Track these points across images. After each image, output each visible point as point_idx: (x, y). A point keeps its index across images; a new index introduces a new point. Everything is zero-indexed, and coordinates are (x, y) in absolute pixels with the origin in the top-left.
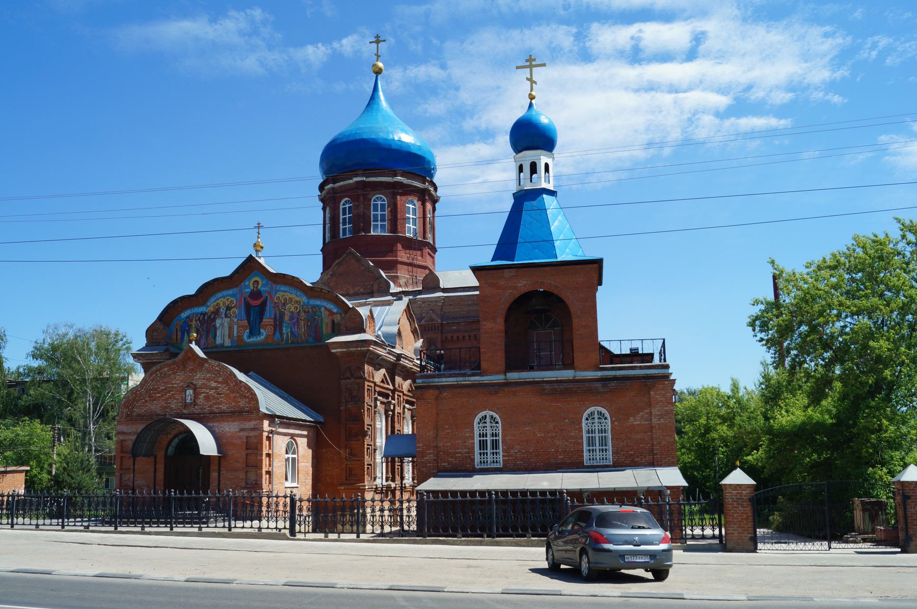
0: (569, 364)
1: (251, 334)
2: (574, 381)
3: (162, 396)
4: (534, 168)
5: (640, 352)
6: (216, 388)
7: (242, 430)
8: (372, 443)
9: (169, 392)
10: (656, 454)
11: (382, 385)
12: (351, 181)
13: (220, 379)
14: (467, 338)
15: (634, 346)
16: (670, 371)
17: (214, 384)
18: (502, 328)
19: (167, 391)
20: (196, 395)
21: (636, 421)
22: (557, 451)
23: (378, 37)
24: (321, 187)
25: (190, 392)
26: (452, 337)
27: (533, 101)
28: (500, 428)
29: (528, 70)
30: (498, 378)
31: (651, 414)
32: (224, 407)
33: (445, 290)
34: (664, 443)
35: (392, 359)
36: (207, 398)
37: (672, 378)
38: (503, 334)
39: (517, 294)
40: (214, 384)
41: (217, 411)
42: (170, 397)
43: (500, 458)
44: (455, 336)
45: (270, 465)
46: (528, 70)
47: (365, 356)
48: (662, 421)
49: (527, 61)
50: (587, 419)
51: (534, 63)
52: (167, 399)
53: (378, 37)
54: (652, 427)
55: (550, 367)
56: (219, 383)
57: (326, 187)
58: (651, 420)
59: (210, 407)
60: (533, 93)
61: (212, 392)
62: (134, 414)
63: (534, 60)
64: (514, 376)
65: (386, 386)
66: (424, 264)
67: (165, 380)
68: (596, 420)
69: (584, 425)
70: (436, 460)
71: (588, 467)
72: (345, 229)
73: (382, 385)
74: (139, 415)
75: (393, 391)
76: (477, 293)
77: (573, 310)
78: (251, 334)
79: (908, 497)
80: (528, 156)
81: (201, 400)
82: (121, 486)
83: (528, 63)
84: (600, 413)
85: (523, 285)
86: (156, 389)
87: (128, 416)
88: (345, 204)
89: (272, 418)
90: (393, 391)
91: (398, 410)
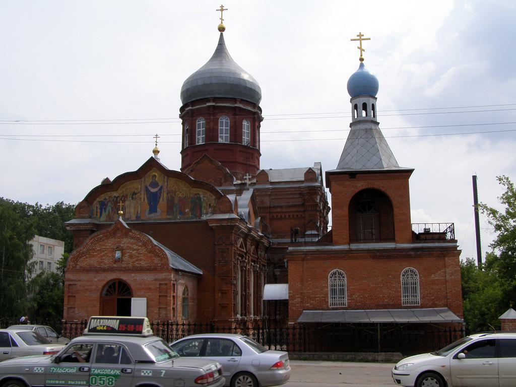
0: (392, 239)
1: (151, 212)
2: (395, 250)
3: (98, 254)
4: (365, 107)
5: (431, 232)
6: (138, 250)
7: (156, 280)
8: (235, 290)
10: (449, 299)
11: (240, 249)
12: (203, 106)
13: (140, 244)
14: (287, 217)
15: (427, 227)
17: (135, 247)
18: (347, 214)
20: (123, 254)
22: (383, 297)
23: (222, 6)
24: (182, 109)
26: (281, 216)
27: (363, 62)
28: (346, 281)
29: (359, 41)
30: (345, 247)
33: (272, 183)
34: (454, 291)
35: (246, 231)
36: (131, 256)
37: (458, 249)
39: (357, 191)
40: (135, 247)
41: (138, 265)
42: (104, 255)
43: (346, 300)
44: (279, 215)
45: (174, 304)
46: (359, 41)
47: (233, 229)
49: (358, 36)
50: (331, 277)
51: (362, 37)
52: (102, 256)
53: (222, 6)
54: (446, 281)
55: (370, 240)
56: (139, 246)
57: (187, 109)
60: (363, 57)
63: (363, 35)
64: (354, 246)
65: (242, 250)
66: (253, 164)
67: (100, 243)
68: (337, 278)
69: (401, 279)
70: (302, 302)
72: (200, 140)
73: (240, 249)
75: (246, 254)
77: (394, 203)
78: (151, 212)
80: (360, 101)
81: (126, 258)
83: (359, 38)
84: (340, 274)
85: (361, 185)
86: (94, 250)
87: (74, 267)
88: (201, 122)
89: (177, 271)
90: (246, 254)
91: (248, 267)
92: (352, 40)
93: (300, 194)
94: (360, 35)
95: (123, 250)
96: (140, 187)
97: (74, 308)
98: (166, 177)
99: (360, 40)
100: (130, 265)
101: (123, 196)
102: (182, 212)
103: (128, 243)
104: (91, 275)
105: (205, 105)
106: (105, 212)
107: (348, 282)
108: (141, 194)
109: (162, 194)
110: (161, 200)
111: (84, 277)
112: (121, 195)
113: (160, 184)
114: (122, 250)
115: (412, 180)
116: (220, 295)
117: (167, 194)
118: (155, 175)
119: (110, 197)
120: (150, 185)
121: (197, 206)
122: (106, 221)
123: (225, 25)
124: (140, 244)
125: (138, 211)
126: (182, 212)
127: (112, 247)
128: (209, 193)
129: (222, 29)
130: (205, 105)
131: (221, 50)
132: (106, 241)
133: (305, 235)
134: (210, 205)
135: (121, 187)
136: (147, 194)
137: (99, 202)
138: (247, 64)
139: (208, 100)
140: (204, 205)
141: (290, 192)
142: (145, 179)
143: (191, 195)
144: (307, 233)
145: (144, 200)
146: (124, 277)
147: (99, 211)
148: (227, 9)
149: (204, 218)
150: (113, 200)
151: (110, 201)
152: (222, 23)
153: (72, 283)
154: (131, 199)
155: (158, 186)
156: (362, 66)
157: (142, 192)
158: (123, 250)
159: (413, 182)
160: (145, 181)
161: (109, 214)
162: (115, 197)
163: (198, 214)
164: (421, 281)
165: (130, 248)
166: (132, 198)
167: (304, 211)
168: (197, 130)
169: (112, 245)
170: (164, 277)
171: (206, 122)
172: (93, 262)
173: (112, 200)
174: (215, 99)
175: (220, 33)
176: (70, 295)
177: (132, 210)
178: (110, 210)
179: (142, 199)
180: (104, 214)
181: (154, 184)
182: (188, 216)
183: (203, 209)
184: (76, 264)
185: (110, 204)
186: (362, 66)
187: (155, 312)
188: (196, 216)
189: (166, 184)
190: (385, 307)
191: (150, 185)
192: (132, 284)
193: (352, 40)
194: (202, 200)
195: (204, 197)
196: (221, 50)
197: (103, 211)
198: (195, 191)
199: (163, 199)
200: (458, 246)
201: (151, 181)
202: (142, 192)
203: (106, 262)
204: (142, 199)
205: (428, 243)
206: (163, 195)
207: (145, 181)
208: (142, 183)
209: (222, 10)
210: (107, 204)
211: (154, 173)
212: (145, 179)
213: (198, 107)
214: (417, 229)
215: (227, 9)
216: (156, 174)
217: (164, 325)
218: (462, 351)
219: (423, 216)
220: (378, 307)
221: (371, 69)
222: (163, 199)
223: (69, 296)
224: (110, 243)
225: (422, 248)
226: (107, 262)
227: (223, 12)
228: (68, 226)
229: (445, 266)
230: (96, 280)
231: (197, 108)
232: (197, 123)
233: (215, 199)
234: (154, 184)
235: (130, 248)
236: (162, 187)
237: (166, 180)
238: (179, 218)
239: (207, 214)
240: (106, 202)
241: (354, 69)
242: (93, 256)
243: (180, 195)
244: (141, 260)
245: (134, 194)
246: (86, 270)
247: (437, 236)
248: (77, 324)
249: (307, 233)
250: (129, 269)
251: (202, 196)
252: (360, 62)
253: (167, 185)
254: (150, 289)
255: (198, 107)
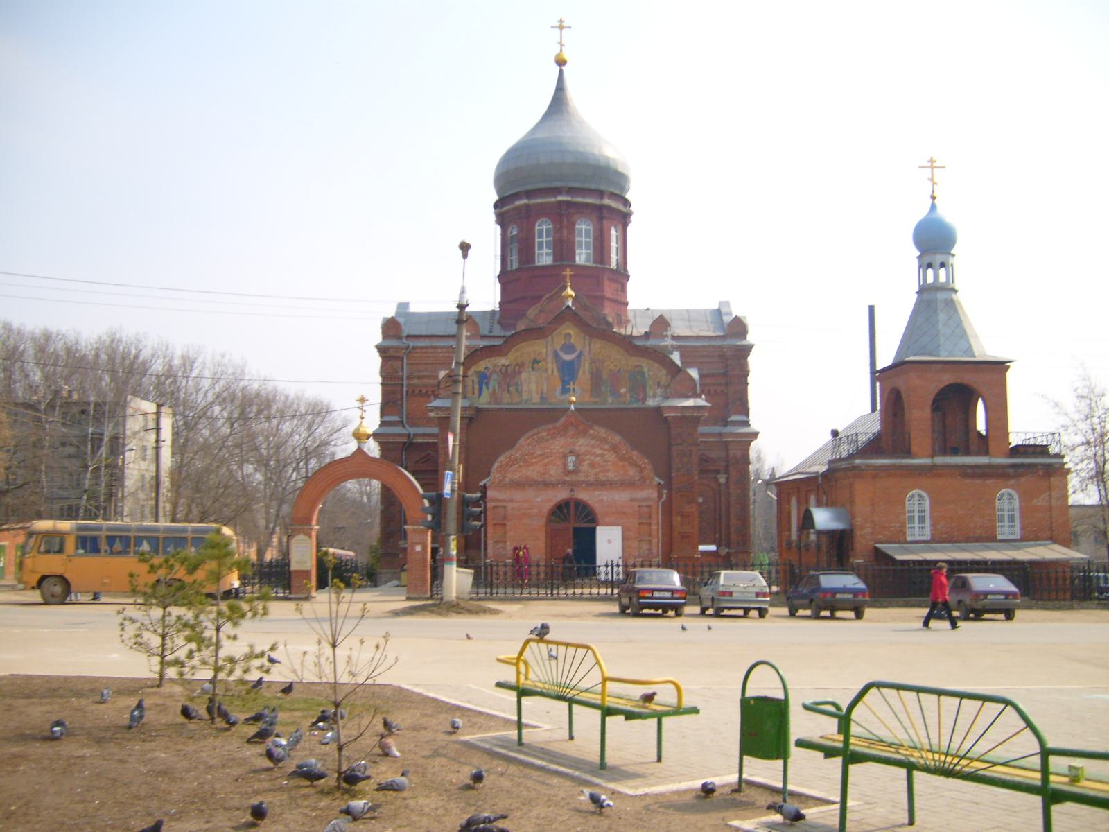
2: (990, 466)
6: (602, 456)
9: (547, 457)
16: (1065, 460)
17: (599, 452)
19: (544, 456)
21: (1040, 502)
23: (561, 21)
25: (571, 459)
30: (926, 461)
31: (1050, 496)
32: (611, 475)
36: (592, 465)
38: (930, 422)
40: (599, 452)
41: (603, 479)
48: (1059, 503)
52: (545, 465)
53: (561, 21)
56: (605, 450)
58: (1050, 501)
59: (596, 474)
61: (598, 459)
62: (507, 480)
64: (940, 460)
70: (872, 533)
71: (1002, 541)
74: (512, 481)
76: (878, 384)
79: (384, 637)
81: (585, 467)
82: (254, 579)
85: (947, 379)
86: (532, 454)
92: (920, 167)
93: (720, 356)
94: (932, 161)
95: (579, 455)
96: (544, 351)
97: (505, 542)
98: (587, 338)
99: (932, 167)
100: (592, 479)
101: (517, 365)
102: (615, 393)
103: (588, 445)
104: (529, 493)
105: (553, 200)
106: (488, 388)
107: (931, 507)
108: (547, 363)
109: (582, 364)
110: (580, 373)
111: (518, 495)
112: (514, 363)
113: (579, 348)
114: (578, 456)
115: (1010, 375)
116: (679, 519)
117: (591, 364)
118: (569, 335)
119: (495, 366)
120: (561, 349)
121: (639, 386)
122: (489, 403)
123: (566, 56)
124: (606, 447)
125: (542, 390)
126: (615, 393)
127: (561, 451)
128: (656, 365)
129: (561, 62)
130: (553, 200)
131: (559, 102)
132: (551, 442)
133: (727, 422)
134: (659, 383)
135: (513, 350)
136: (557, 362)
137: (476, 372)
138: (609, 130)
139: (557, 191)
140: (650, 383)
141: (704, 354)
142: (553, 339)
143: (630, 368)
144: (730, 419)
145: (553, 372)
146: (583, 495)
147: (477, 386)
148: (570, 27)
149: (651, 403)
150: (501, 370)
151: (495, 371)
152: (561, 50)
153: (499, 504)
154: (530, 369)
155: (575, 351)
156: (933, 207)
157: (550, 359)
158: (579, 455)
159: (1012, 378)
160: (552, 342)
161: (494, 393)
162: (504, 365)
163: (640, 397)
164: (1021, 508)
165: (590, 453)
166: (533, 369)
167: (727, 384)
168: (537, 240)
169: (562, 447)
170: (646, 496)
171: (555, 228)
172: (532, 472)
173: (498, 370)
174: (570, 191)
175: (558, 68)
176: (495, 522)
177: (533, 387)
178: (496, 386)
179: (550, 371)
180: (485, 393)
181: (569, 348)
182: (624, 398)
183: (648, 389)
184: (504, 477)
185: (495, 376)
186: (933, 207)
187: (634, 546)
188: (638, 400)
189: (588, 348)
190: (977, 540)
191: (561, 349)
192: (598, 508)
193: (920, 167)
194: (646, 375)
195: (649, 370)
196: (559, 102)
197: (484, 386)
198: (634, 361)
199: (584, 372)
200: (1066, 463)
201: (563, 342)
202: (550, 359)
203: (553, 472)
204: (550, 371)
205: (1029, 457)
206: (584, 366)
207: (552, 342)
208: (549, 346)
209: (561, 27)
210: (490, 376)
211: (567, 331)
212: (553, 339)
213: (539, 201)
214: (1015, 440)
215: (570, 27)
216: (572, 333)
217: (607, 566)
218: (332, 579)
219: (1023, 425)
220: (968, 540)
221: (947, 213)
222: (584, 372)
223: (494, 524)
224: (558, 445)
225: (1022, 465)
226: (554, 472)
227: (563, 31)
228: (432, 411)
229: (1050, 489)
230: (539, 500)
231: (538, 204)
232: (537, 228)
233: (667, 375)
234: (569, 348)
235: (590, 453)
236: (580, 354)
237: (587, 343)
238: (610, 402)
239: (654, 396)
240: (488, 374)
241: (922, 212)
242: (532, 464)
243: (612, 367)
244: (607, 471)
245: (535, 361)
246: (518, 485)
247: (1031, 450)
248: (564, 568)
249: (730, 419)
250: (592, 484)
251: (646, 370)
252: (931, 200)
253: (590, 350)
254: (624, 513)
255: (539, 201)
